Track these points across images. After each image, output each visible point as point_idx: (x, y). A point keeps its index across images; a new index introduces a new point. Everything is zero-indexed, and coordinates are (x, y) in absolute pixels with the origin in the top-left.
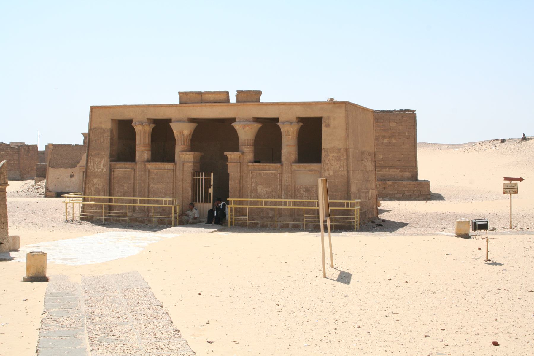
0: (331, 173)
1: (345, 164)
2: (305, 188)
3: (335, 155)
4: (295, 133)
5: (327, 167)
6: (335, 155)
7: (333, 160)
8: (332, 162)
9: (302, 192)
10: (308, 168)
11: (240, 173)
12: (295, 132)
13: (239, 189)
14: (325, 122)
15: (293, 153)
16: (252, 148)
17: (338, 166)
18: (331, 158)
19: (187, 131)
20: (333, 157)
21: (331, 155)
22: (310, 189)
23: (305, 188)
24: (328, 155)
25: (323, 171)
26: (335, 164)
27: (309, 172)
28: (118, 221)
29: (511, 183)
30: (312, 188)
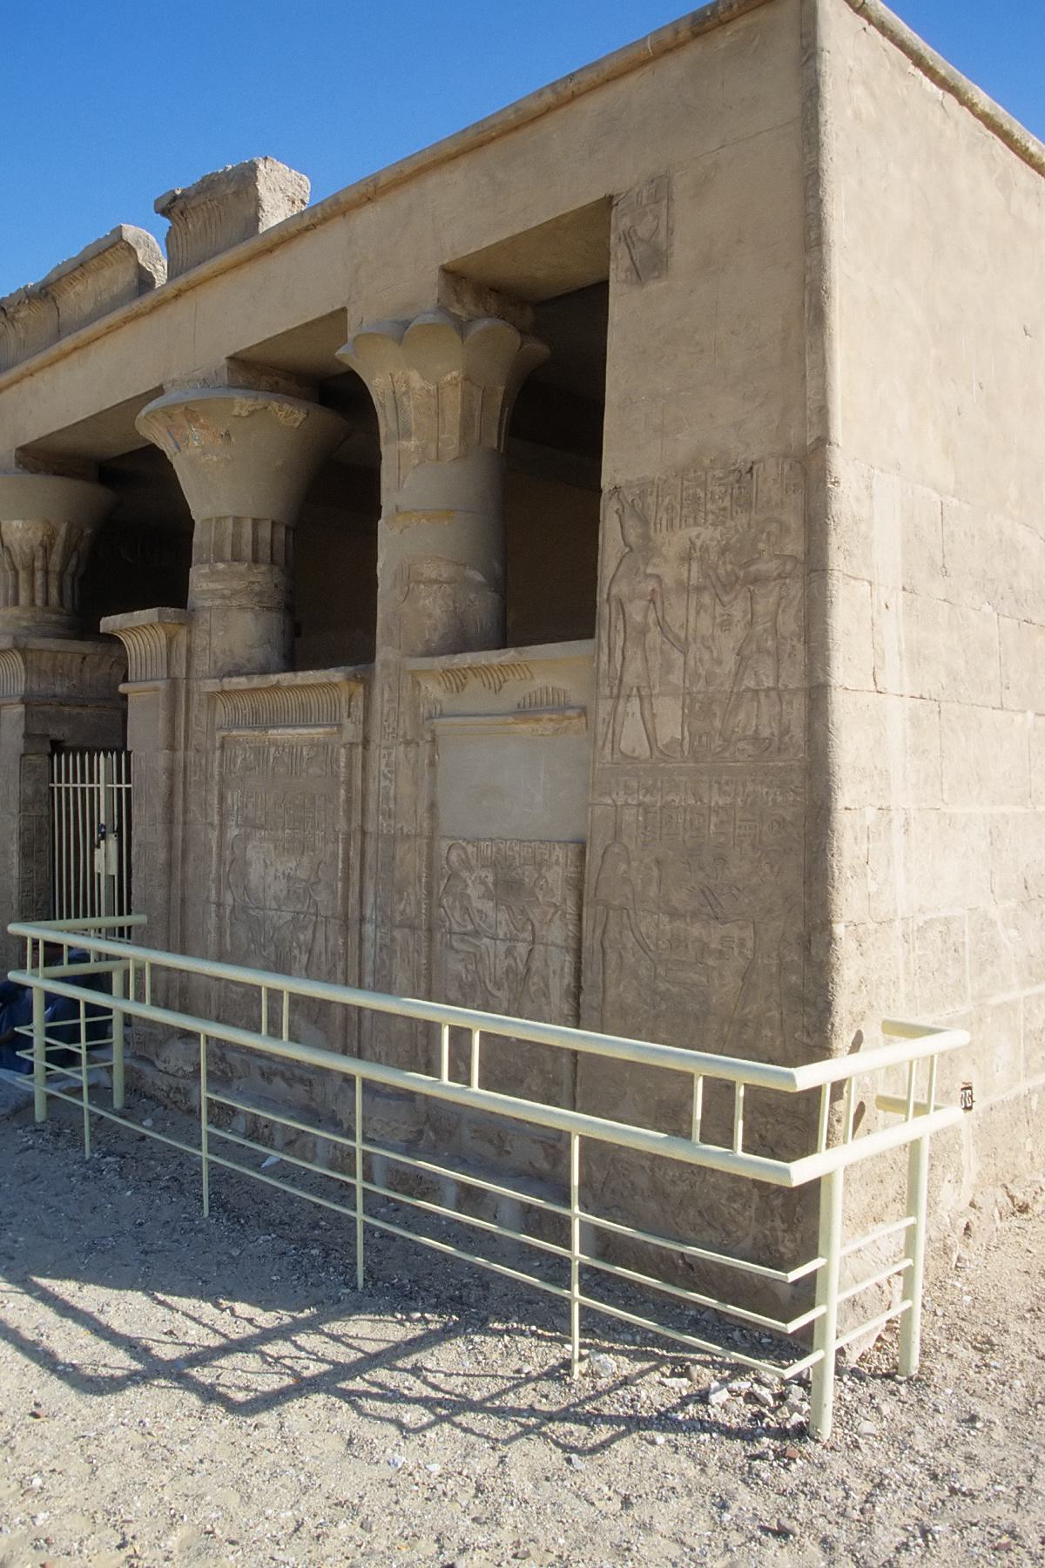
0: (671, 728)
1: (789, 623)
2: (494, 864)
3: (707, 534)
4: (453, 416)
5: (635, 668)
6: (707, 534)
7: (684, 588)
8: (677, 612)
9: (473, 891)
10: (517, 690)
11: (172, 747)
12: (453, 400)
13: (162, 856)
14: (628, 238)
15: (429, 571)
16: (262, 577)
17: (728, 644)
18: (669, 571)
19: (17, 523)
20: (687, 558)
21: (672, 541)
22: (528, 875)
23: (494, 864)
24: (647, 549)
25: (605, 707)
26: (705, 624)
27: (525, 728)
28: (806, 944)
29: (371, 921)
30: (540, 865)
